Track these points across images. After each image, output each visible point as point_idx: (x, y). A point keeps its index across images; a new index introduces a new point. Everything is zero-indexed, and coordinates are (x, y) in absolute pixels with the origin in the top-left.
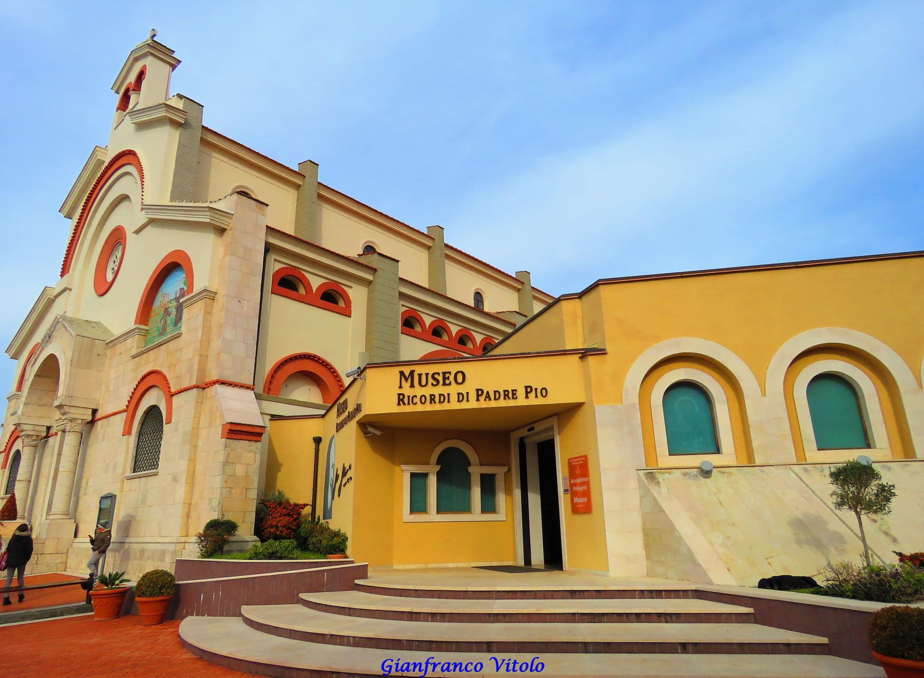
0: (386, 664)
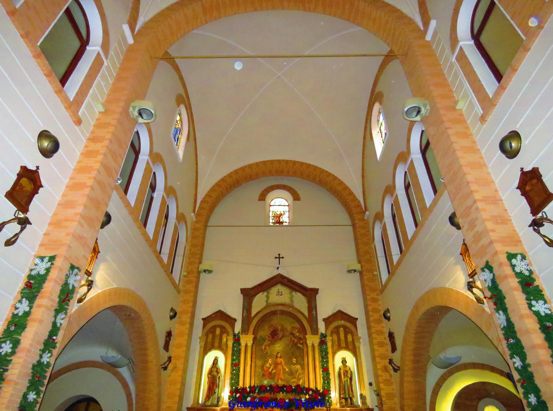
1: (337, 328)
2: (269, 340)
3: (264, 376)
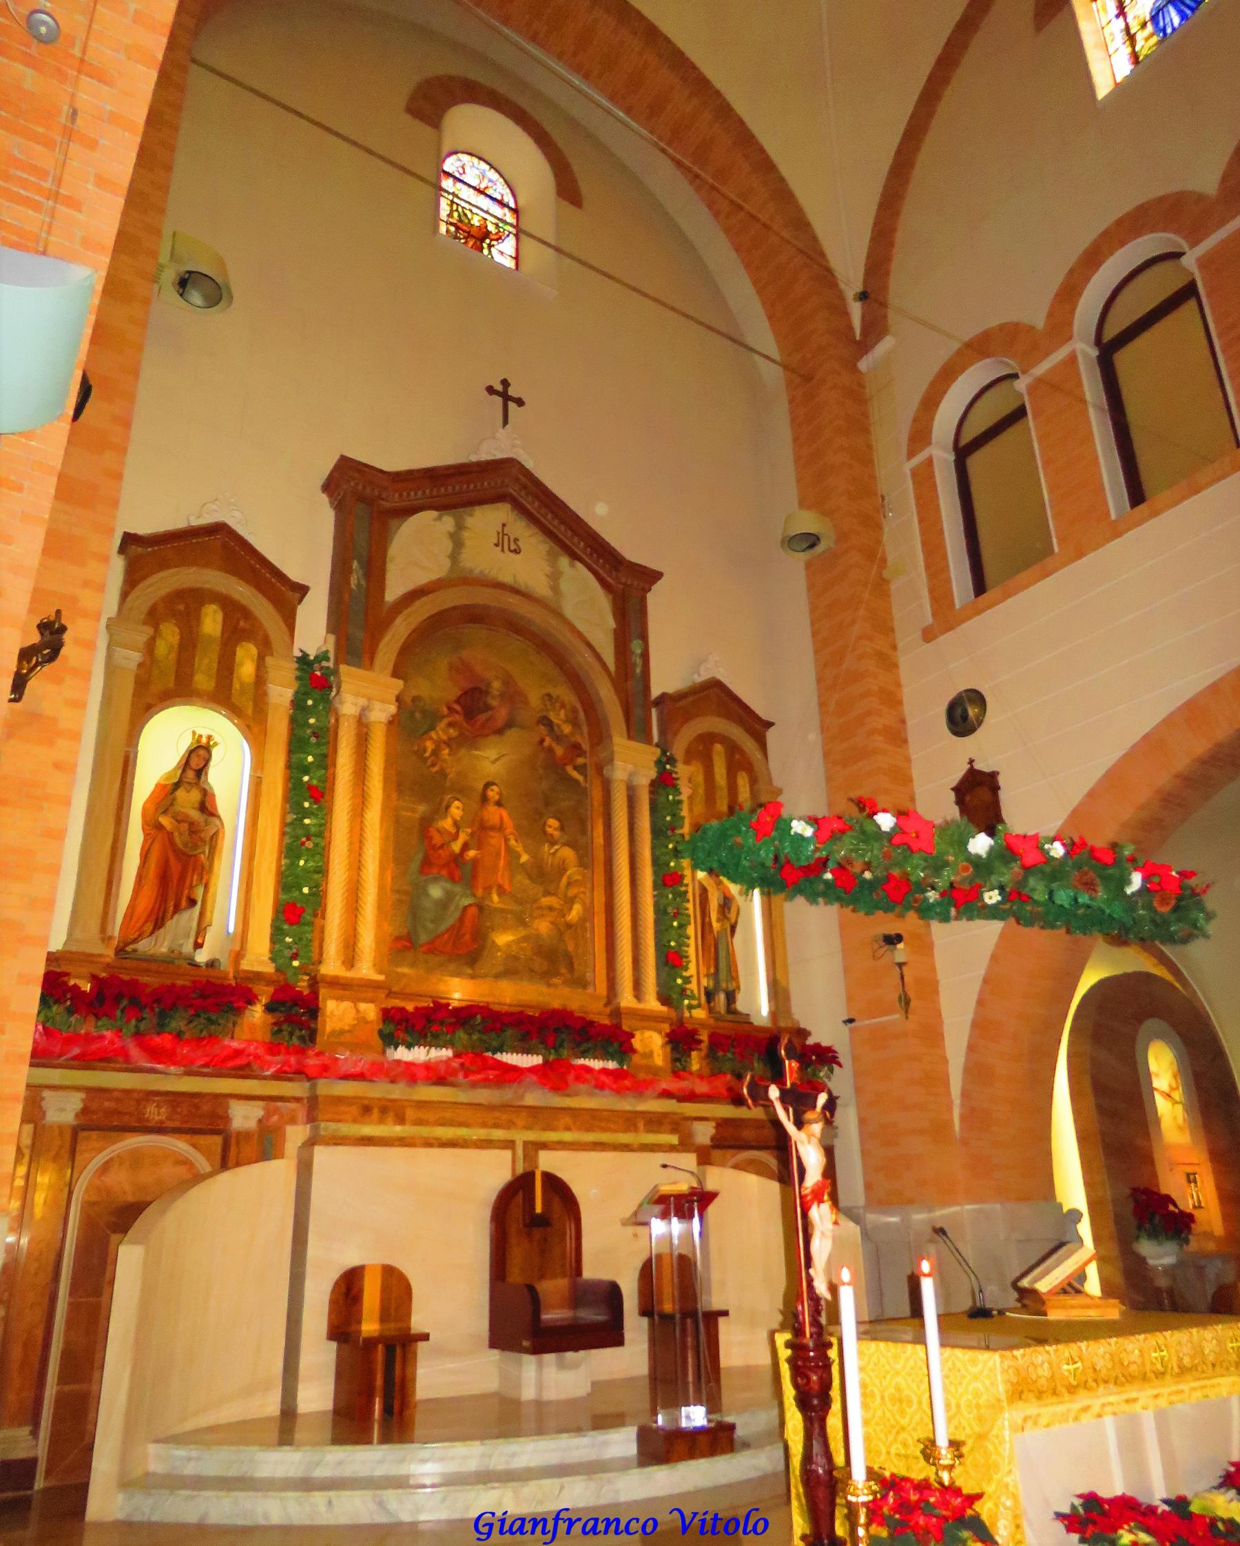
0: (481, 1523)
1: (708, 739)
2: (450, 725)
3: (426, 864)
